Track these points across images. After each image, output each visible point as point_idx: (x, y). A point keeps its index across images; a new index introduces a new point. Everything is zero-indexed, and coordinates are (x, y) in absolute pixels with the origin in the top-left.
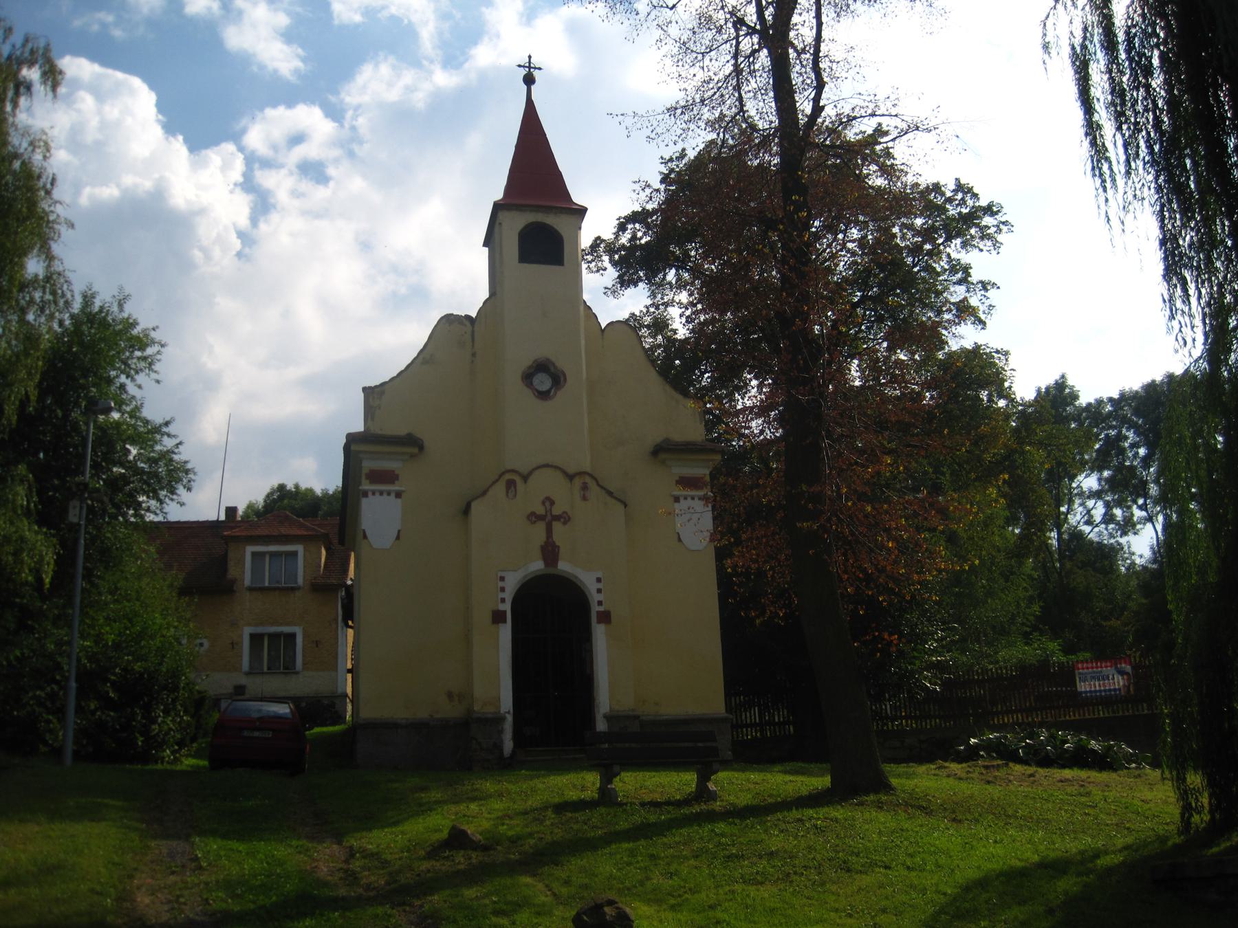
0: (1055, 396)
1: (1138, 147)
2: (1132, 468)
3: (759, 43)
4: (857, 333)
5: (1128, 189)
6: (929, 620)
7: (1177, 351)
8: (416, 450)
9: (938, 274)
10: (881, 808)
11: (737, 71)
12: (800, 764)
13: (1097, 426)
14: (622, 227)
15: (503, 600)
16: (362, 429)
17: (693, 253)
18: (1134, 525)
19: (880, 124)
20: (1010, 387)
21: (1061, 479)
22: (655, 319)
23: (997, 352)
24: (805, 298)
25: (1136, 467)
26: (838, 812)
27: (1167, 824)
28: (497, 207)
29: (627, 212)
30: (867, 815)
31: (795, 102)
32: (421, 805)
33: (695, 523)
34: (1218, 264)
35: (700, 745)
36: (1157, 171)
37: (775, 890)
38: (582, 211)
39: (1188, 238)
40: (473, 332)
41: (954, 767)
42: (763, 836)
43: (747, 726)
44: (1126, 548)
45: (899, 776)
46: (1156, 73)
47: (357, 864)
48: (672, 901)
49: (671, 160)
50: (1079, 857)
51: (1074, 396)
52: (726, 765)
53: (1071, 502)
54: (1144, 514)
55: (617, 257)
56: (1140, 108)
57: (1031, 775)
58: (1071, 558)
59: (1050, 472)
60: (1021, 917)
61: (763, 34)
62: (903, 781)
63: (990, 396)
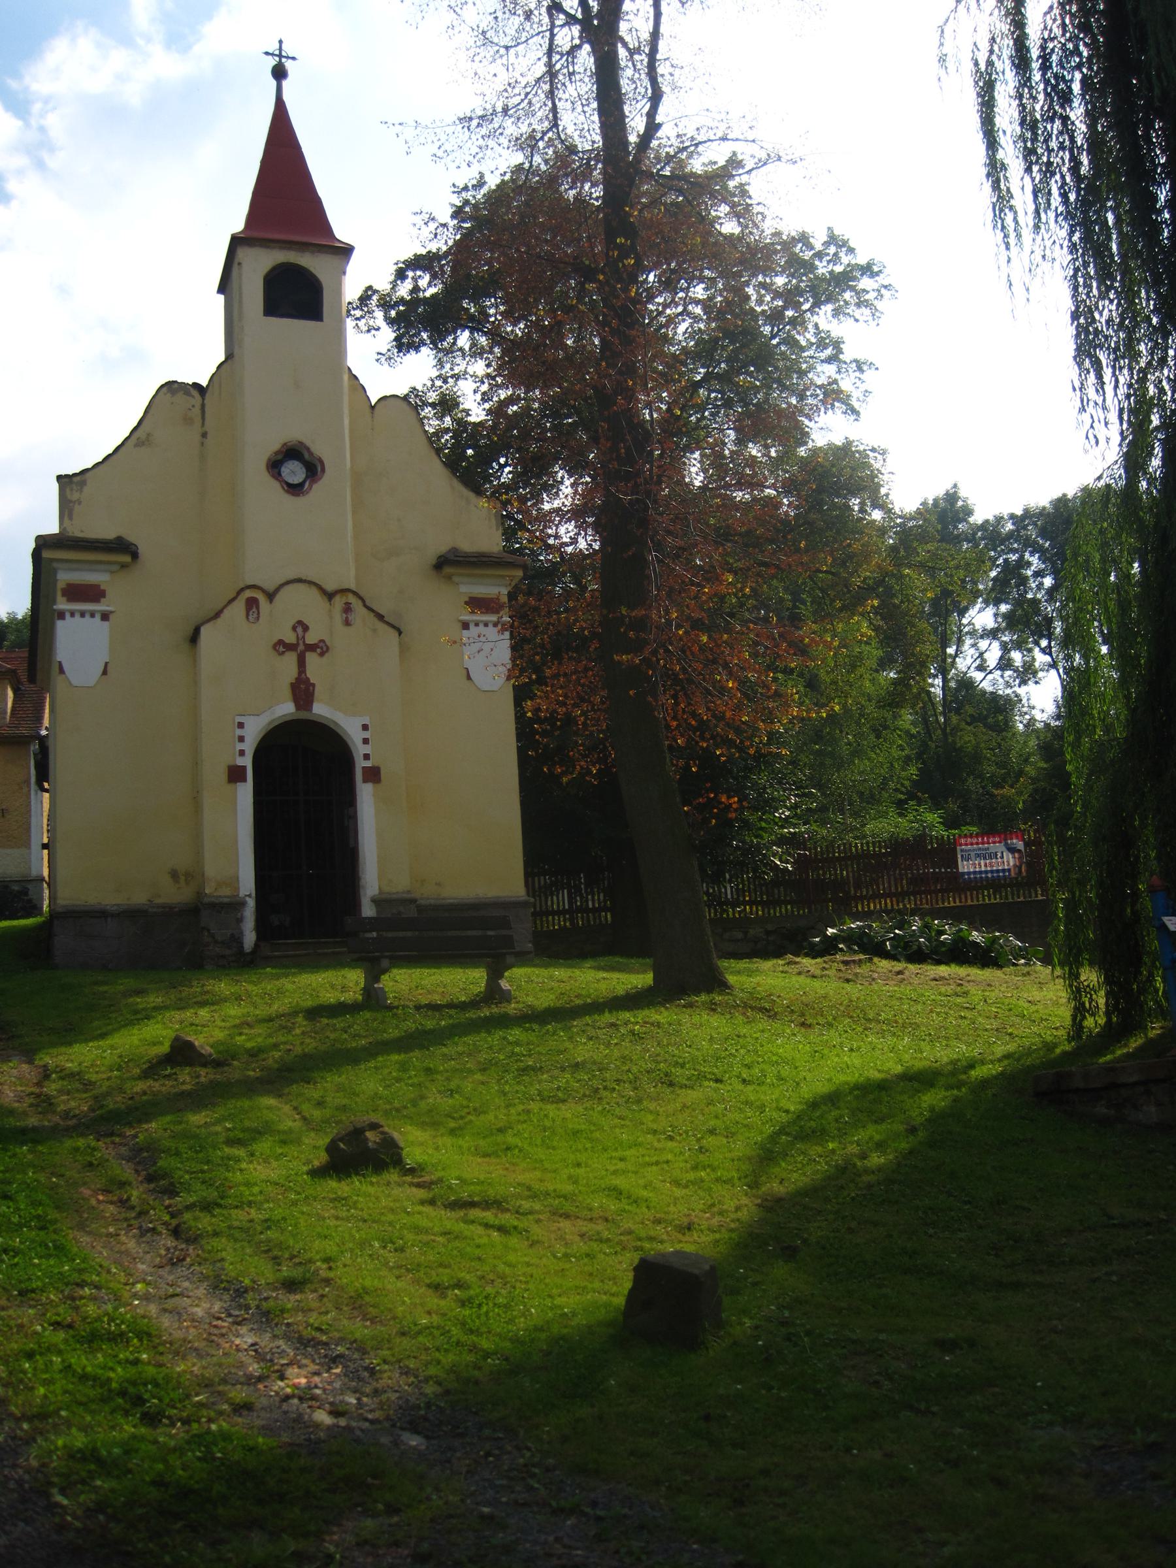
0: (944, 511)
1: (1049, 193)
2: (1035, 602)
3: (580, 37)
4: (699, 420)
5: (1036, 248)
6: (780, 783)
7: (1086, 451)
8: (127, 559)
9: (803, 349)
10: (714, 1010)
11: (551, 73)
12: (617, 959)
13: (995, 550)
14: (401, 275)
15: (242, 753)
16: (57, 531)
17: (492, 311)
18: (1035, 673)
19: (734, 154)
20: (887, 495)
21: (948, 613)
22: (443, 395)
23: (873, 450)
24: (630, 370)
25: (1040, 601)
26: (661, 1015)
27: (1056, 1029)
28: (236, 242)
29: (408, 255)
30: (696, 1019)
31: (623, 116)
32: (136, 1012)
33: (489, 655)
34: (1142, 347)
35: (490, 933)
36: (1071, 226)
37: (580, 1109)
38: (346, 251)
39: (1106, 313)
40: (203, 406)
41: (807, 962)
42: (567, 1044)
43: (553, 913)
44: (1024, 701)
45: (739, 972)
46: (1076, 103)
47: (53, 1086)
48: (452, 1124)
49: (466, 188)
50: (950, 1068)
51: (968, 511)
52: (523, 959)
53: (960, 642)
54: (1048, 659)
55: (393, 313)
56: (1054, 144)
57: (900, 973)
58: (958, 711)
59: (935, 602)
60: (877, 1137)
61: (585, 23)
62: (744, 978)
63: (862, 504)
